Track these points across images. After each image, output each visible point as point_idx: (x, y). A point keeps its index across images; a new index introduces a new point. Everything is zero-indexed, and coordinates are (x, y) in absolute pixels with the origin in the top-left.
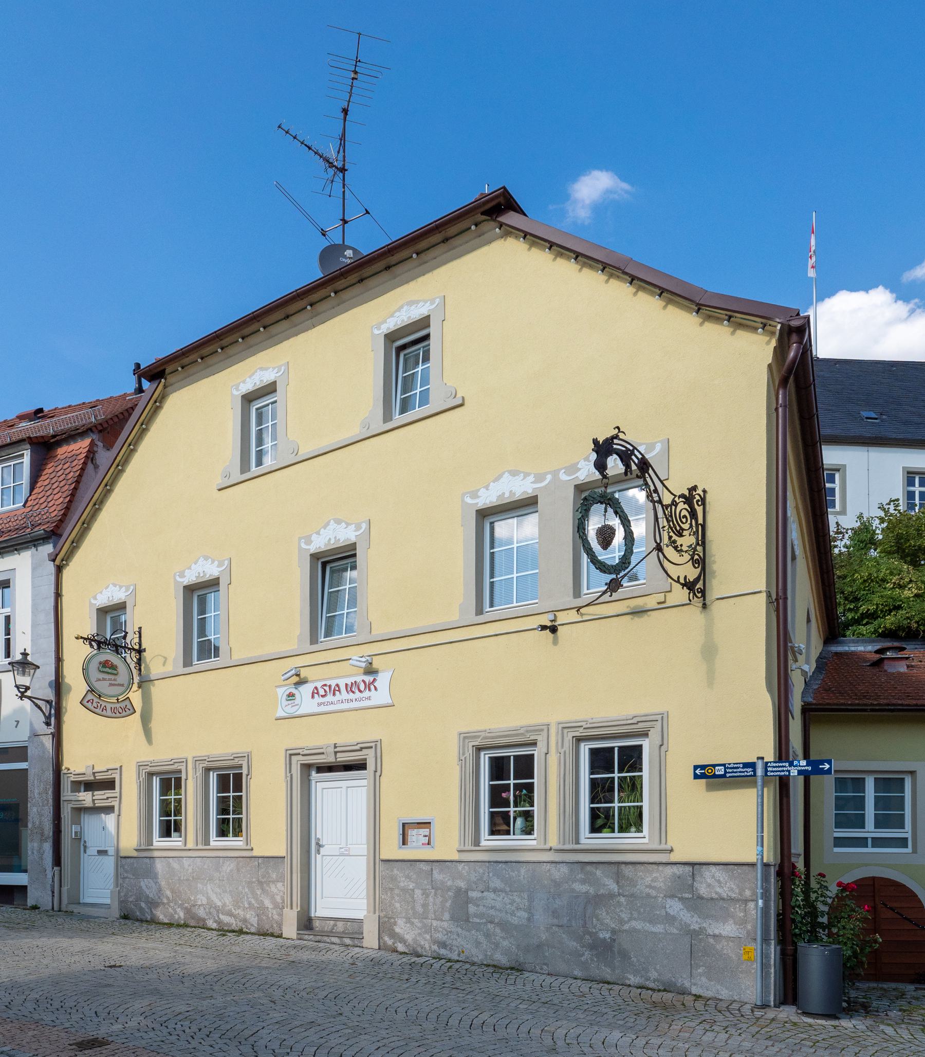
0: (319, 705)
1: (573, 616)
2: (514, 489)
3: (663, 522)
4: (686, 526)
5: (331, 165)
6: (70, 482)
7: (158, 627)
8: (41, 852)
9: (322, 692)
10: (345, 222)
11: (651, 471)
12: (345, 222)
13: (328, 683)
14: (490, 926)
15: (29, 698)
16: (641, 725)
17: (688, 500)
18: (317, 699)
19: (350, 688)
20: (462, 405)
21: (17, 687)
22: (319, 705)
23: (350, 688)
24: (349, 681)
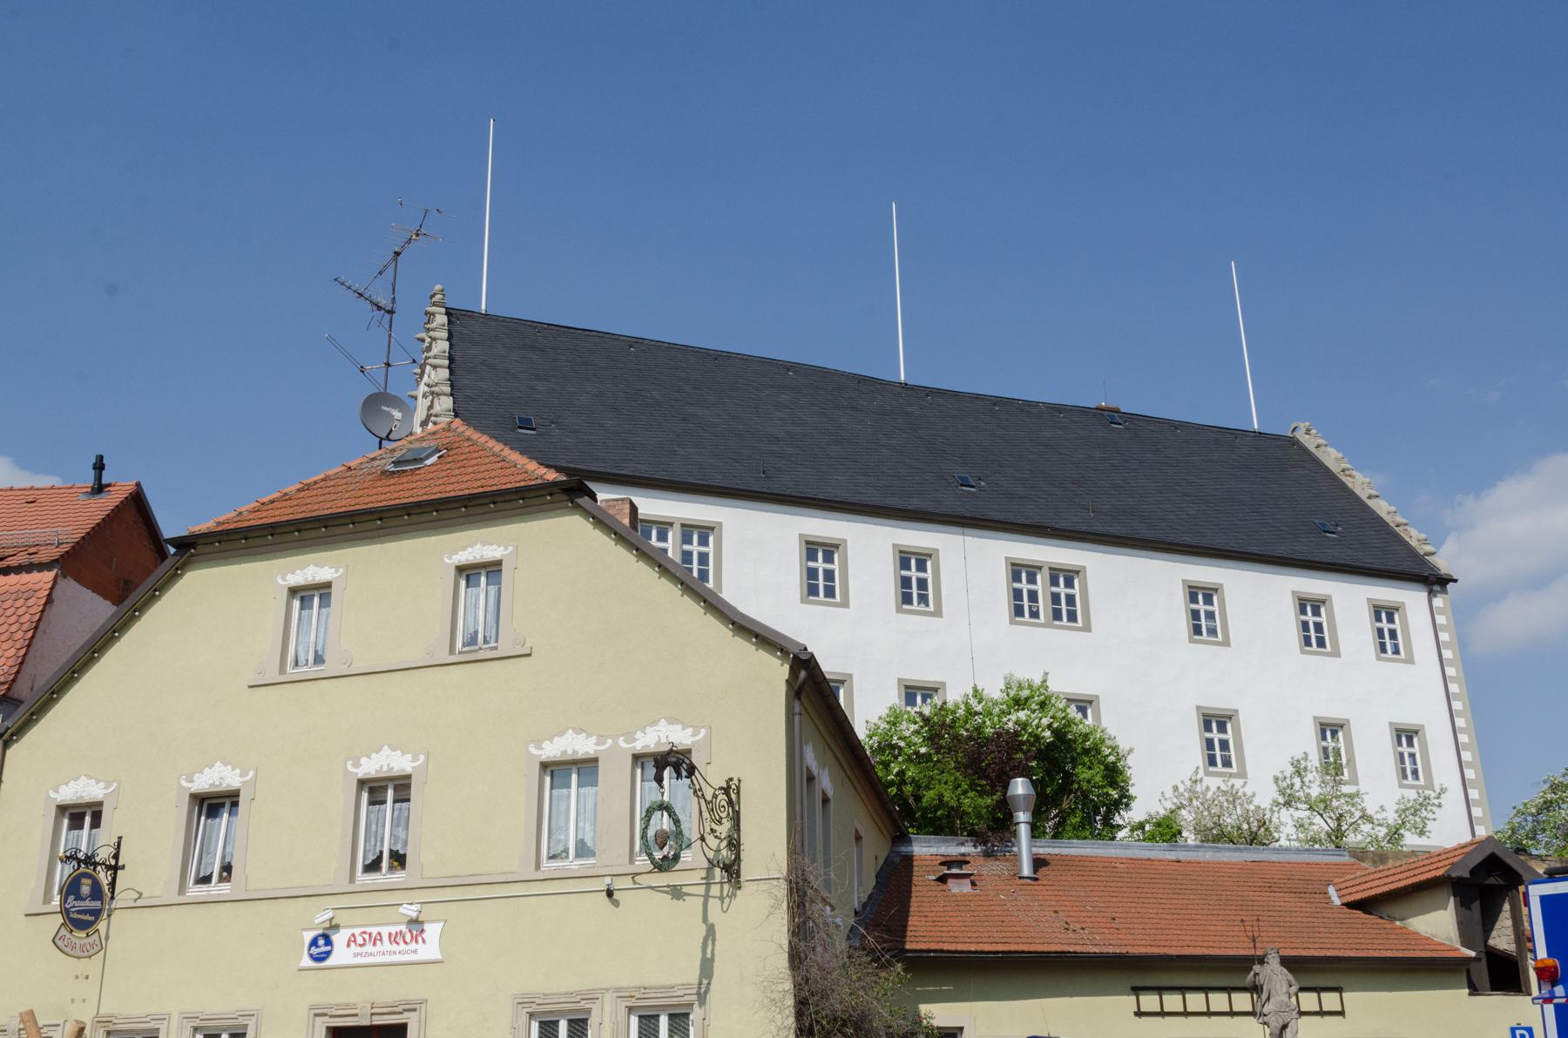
0: (355, 955)
1: (627, 882)
2: (577, 748)
3: (706, 815)
4: (724, 815)
5: (379, 308)
6: (25, 627)
7: (149, 842)
9: (359, 940)
10: (388, 365)
11: (685, 889)
12: (388, 365)
13: (368, 930)
17: (726, 790)
19: (393, 938)
22: (355, 955)
23: (393, 938)
24: (394, 929)
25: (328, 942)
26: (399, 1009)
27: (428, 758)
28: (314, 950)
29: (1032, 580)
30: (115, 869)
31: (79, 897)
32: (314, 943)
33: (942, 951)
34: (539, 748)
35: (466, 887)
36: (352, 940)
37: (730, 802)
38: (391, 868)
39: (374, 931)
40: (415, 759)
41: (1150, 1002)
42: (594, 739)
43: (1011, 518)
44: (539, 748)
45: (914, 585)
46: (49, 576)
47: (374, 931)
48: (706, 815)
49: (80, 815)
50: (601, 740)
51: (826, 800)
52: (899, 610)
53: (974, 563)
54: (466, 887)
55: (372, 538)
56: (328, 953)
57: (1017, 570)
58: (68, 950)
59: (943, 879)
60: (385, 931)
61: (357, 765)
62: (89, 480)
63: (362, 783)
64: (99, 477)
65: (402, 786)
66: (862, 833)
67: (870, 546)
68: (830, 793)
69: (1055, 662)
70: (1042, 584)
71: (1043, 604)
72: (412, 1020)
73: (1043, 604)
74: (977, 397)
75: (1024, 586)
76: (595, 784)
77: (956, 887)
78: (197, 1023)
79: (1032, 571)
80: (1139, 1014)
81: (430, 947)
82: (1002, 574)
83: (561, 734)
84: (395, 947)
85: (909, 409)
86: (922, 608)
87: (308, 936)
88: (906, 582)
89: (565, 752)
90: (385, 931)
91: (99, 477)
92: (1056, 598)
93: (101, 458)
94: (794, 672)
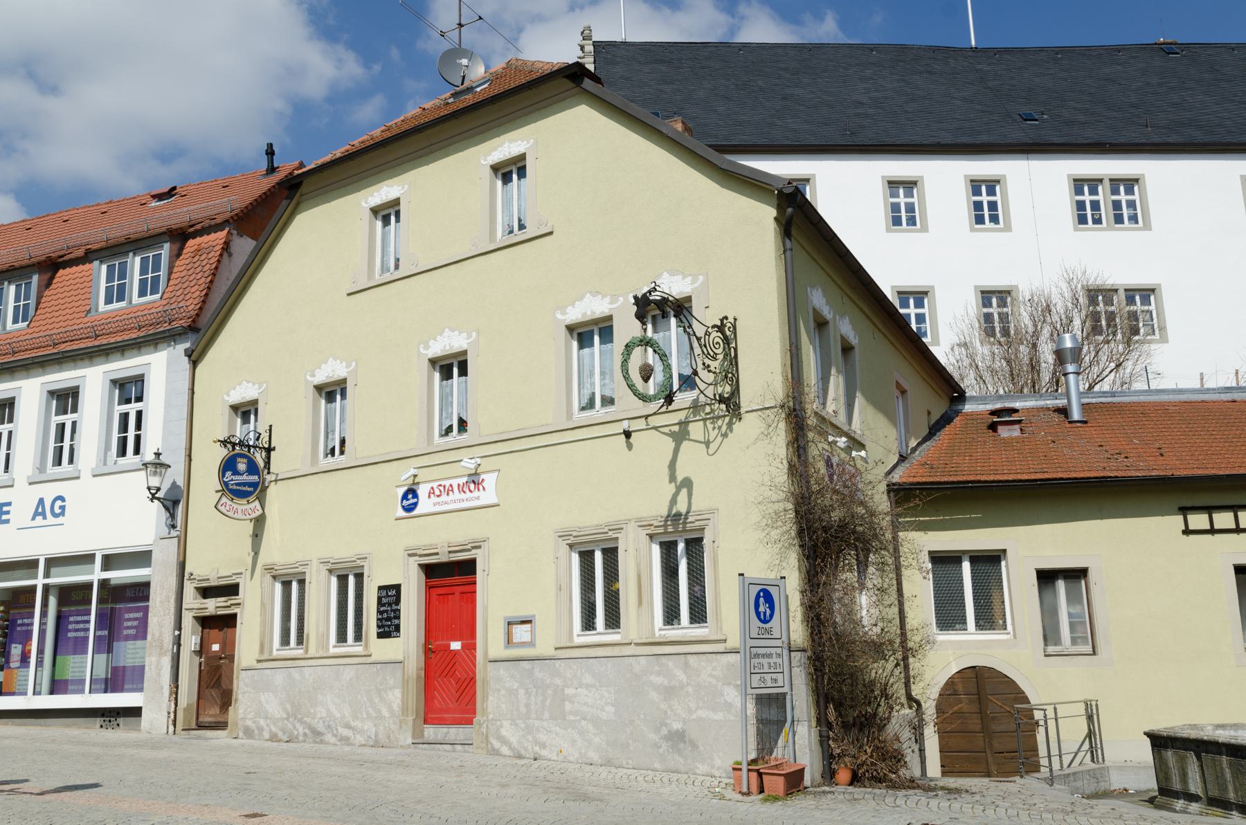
1: (641, 424)
3: (697, 350)
7: (291, 430)
8: (159, 668)
9: (437, 492)
13: (443, 483)
14: (584, 723)
15: (158, 499)
16: (697, 523)
17: (720, 328)
18: (434, 499)
19: (461, 489)
20: (551, 233)
21: (149, 489)
25: (415, 496)
26: (468, 547)
27: (478, 334)
28: (406, 503)
29: (1093, 191)
30: (269, 450)
31: (236, 473)
32: (405, 497)
33: (979, 482)
34: (564, 313)
35: (509, 442)
36: (431, 493)
37: (726, 340)
38: (459, 431)
39: (447, 483)
40: (469, 336)
41: (1199, 520)
42: (608, 299)
43: (1072, 140)
44: (564, 313)
45: (986, 207)
46: (222, 234)
47: (447, 483)
48: (697, 350)
49: (245, 411)
50: (614, 299)
51: (847, 349)
52: (972, 230)
53: (1039, 184)
54: (509, 442)
55: (426, 155)
56: (415, 504)
57: (1079, 184)
58: (230, 514)
59: (993, 427)
60: (455, 482)
61: (427, 347)
62: (264, 166)
63: (433, 362)
64: (271, 161)
65: (1077, 574)
66: (905, 385)
67: (944, 179)
68: (853, 340)
69: (1113, 258)
70: (1103, 195)
71: (1106, 212)
72: (478, 554)
73: (1106, 212)
74: (1042, 49)
75: (1087, 198)
76: (612, 341)
77: (1004, 432)
78: (330, 566)
79: (1093, 183)
80: (1187, 532)
81: (487, 495)
82: (1066, 189)
83: (581, 298)
84: (463, 496)
85: (979, 67)
86: (992, 225)
87: (401, 491)
88: (978, 206)
89: (584, 314)
90: (455, 482)
91: (271, 161)
92: (1117, 205)
93: (270, 146)
94: (780, 209)
